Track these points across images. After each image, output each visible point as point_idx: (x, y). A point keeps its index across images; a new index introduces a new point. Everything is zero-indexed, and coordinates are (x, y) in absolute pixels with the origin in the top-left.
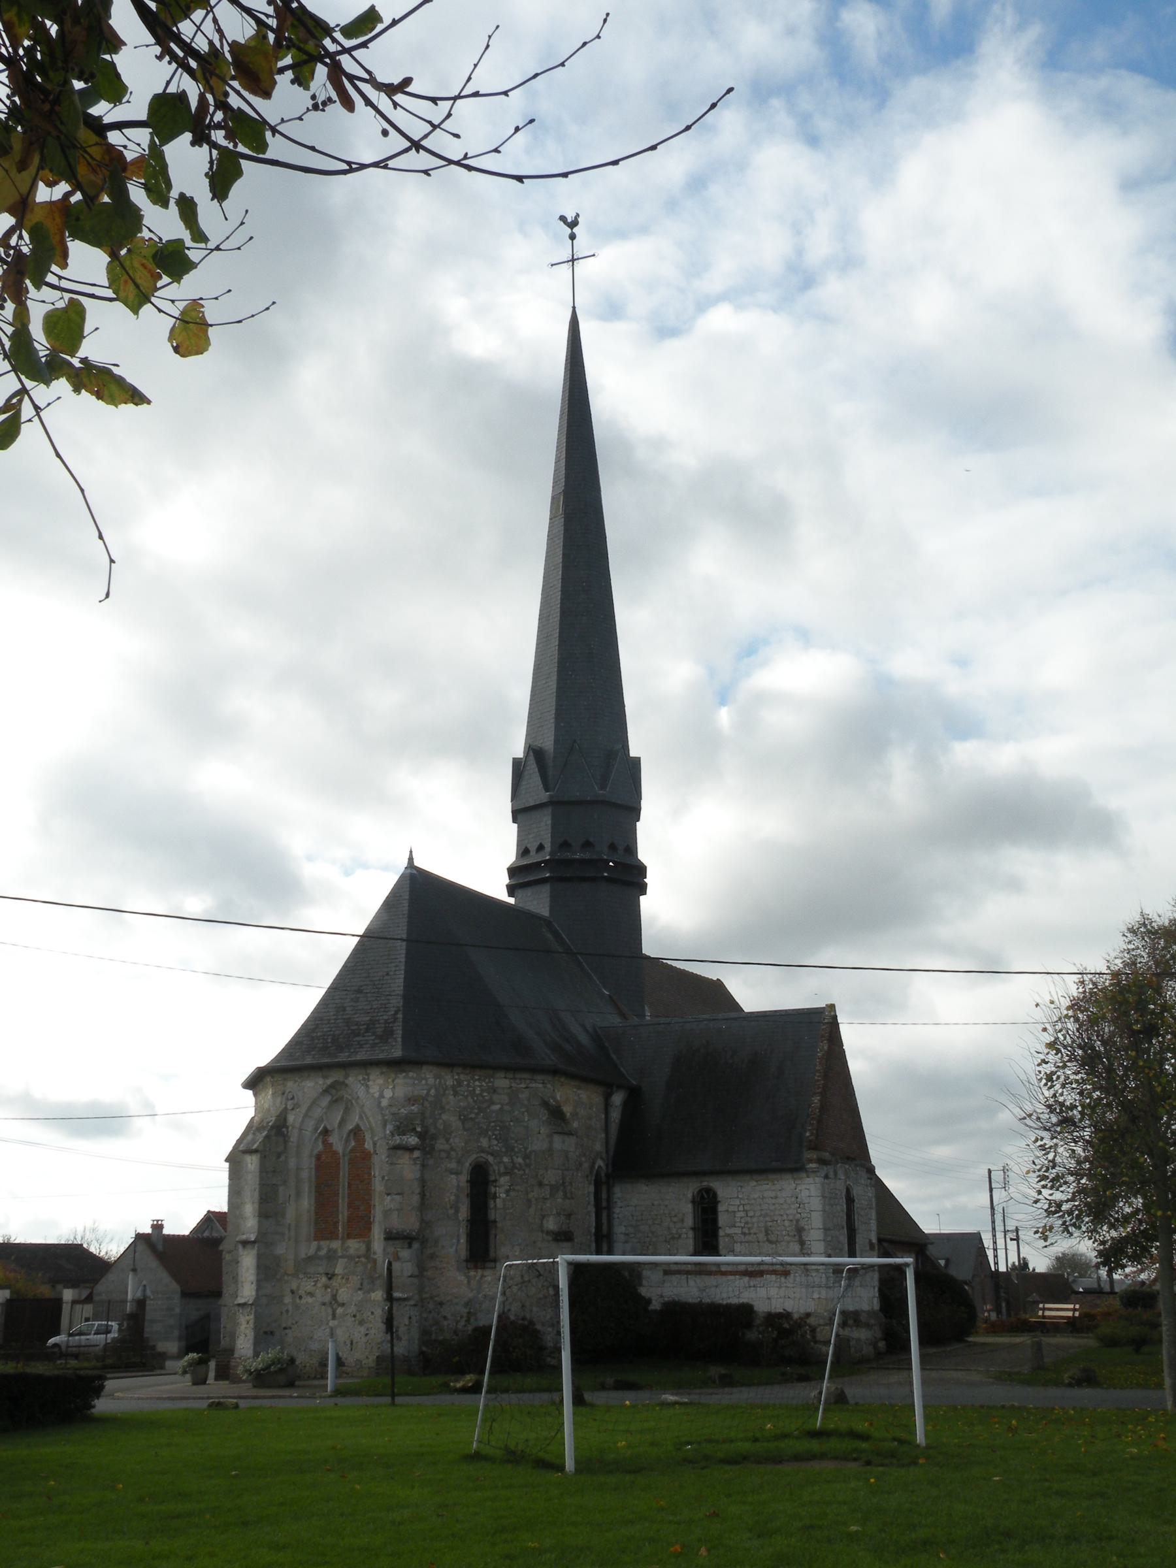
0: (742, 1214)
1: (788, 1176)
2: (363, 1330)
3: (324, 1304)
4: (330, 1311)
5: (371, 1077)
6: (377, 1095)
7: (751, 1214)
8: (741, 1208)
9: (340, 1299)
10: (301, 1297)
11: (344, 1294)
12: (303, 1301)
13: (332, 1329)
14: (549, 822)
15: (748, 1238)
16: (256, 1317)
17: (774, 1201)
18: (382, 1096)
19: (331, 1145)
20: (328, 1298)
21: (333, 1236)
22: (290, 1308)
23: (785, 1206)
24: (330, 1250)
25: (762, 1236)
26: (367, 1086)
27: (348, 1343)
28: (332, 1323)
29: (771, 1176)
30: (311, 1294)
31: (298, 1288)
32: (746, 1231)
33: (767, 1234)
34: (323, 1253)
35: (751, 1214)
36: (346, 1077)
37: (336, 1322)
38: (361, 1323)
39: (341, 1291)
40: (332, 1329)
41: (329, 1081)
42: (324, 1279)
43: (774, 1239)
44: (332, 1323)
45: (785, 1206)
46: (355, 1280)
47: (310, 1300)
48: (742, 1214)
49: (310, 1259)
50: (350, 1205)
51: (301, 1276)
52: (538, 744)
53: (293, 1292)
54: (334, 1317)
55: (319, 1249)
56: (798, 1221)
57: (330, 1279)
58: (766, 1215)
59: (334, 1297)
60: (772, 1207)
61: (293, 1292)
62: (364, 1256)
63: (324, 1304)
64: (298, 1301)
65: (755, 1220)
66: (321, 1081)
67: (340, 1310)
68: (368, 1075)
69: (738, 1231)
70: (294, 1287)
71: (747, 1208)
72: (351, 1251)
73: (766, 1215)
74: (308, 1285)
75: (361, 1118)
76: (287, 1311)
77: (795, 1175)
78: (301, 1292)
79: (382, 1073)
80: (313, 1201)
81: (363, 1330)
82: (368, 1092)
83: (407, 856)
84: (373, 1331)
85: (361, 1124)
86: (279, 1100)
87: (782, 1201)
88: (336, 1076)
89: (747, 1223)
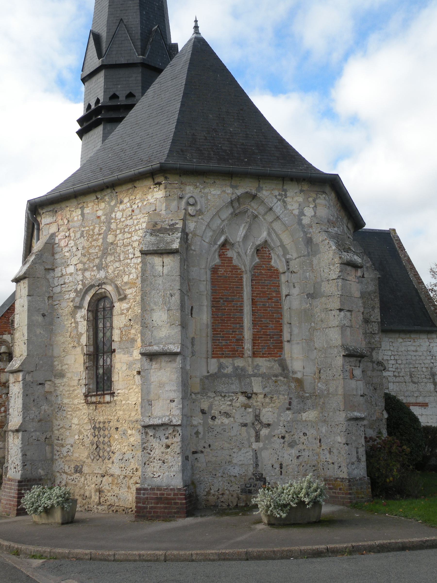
0: (393, 362)
1: (424, 336)
2: (294, 452)
3: (245, 425)
4: (253, 433)
5: (288, 194)
6: (296, 212)
7: (399, 362)
8: (392, 358)
9: (264, 420)
10: (213, 418)
11: (267, 415)
12: (218, 422)
13: (255, 452)
14: (140, 78)
15: (398, 379)
16: (183, 440)
17: (415, 353)
18: (302, 213)
19: (230, 259)
20: (249, 419)
21: (237, 353)
22: (201, 429)
23: (423, 357)
24: (236, 368)
25: (407, 378)
26: (284, 202)
27: (277, 466)
28: (255, 446)
29: (413, 336)
30: (227, 415)
31: (211, 407)
32: (396, 374)
33: (411, 377)
34: (229, 370)
35: (399, 362)
36: (259, 189)
37: (261, 445)
38: (292, 445)
39: (264, 411)
40: (255, 452)
41: (239, 192)
42: (242, 399)
43: (416, 381)
44: (255, 446)
45: (423, 357)
46: (282, 400)
47: (226, 421)
48: (393, 362)
49: (212, 377)
50: (254, 323)
51: (211, 394)
52: (96, 31)
53: (203, 412)
54: (258, 438)
55: (221, 367)
56: (431, 368)
57: (249, 398)
58: (410, 363)
59: (257, 417)
60: (414, 358)
61: (203, 412)
62: (281, 375)
63: (245, 425)
64: (210, 422)
65: (402, 366)
66: (229, 190)
67: (264, 432)
68: (285, 191)
69: (391, 374)
70: (205, 406)
71: (397, 357)
72: (263, 370)
73: (410, 363)
74: (221, 405)
75: (269, 234)
76: (197, 433)
77: (429, 336)
78: (214, 412)
79: (301, 191)
80: (210, 315)
81: (294, 452)
82: (285, 207)
83: (193, 24)
84: (306, 453)
85: (269, 241)
86: (174, 204)
87: (420, 354)
88: (246, 187)
89: (397, 368)
